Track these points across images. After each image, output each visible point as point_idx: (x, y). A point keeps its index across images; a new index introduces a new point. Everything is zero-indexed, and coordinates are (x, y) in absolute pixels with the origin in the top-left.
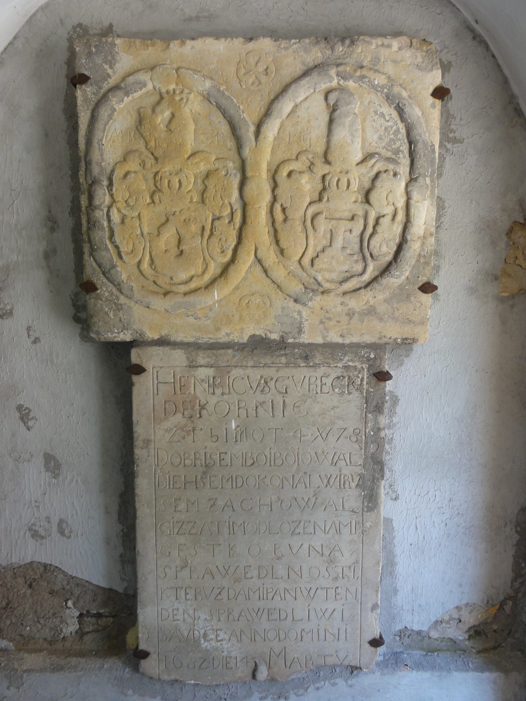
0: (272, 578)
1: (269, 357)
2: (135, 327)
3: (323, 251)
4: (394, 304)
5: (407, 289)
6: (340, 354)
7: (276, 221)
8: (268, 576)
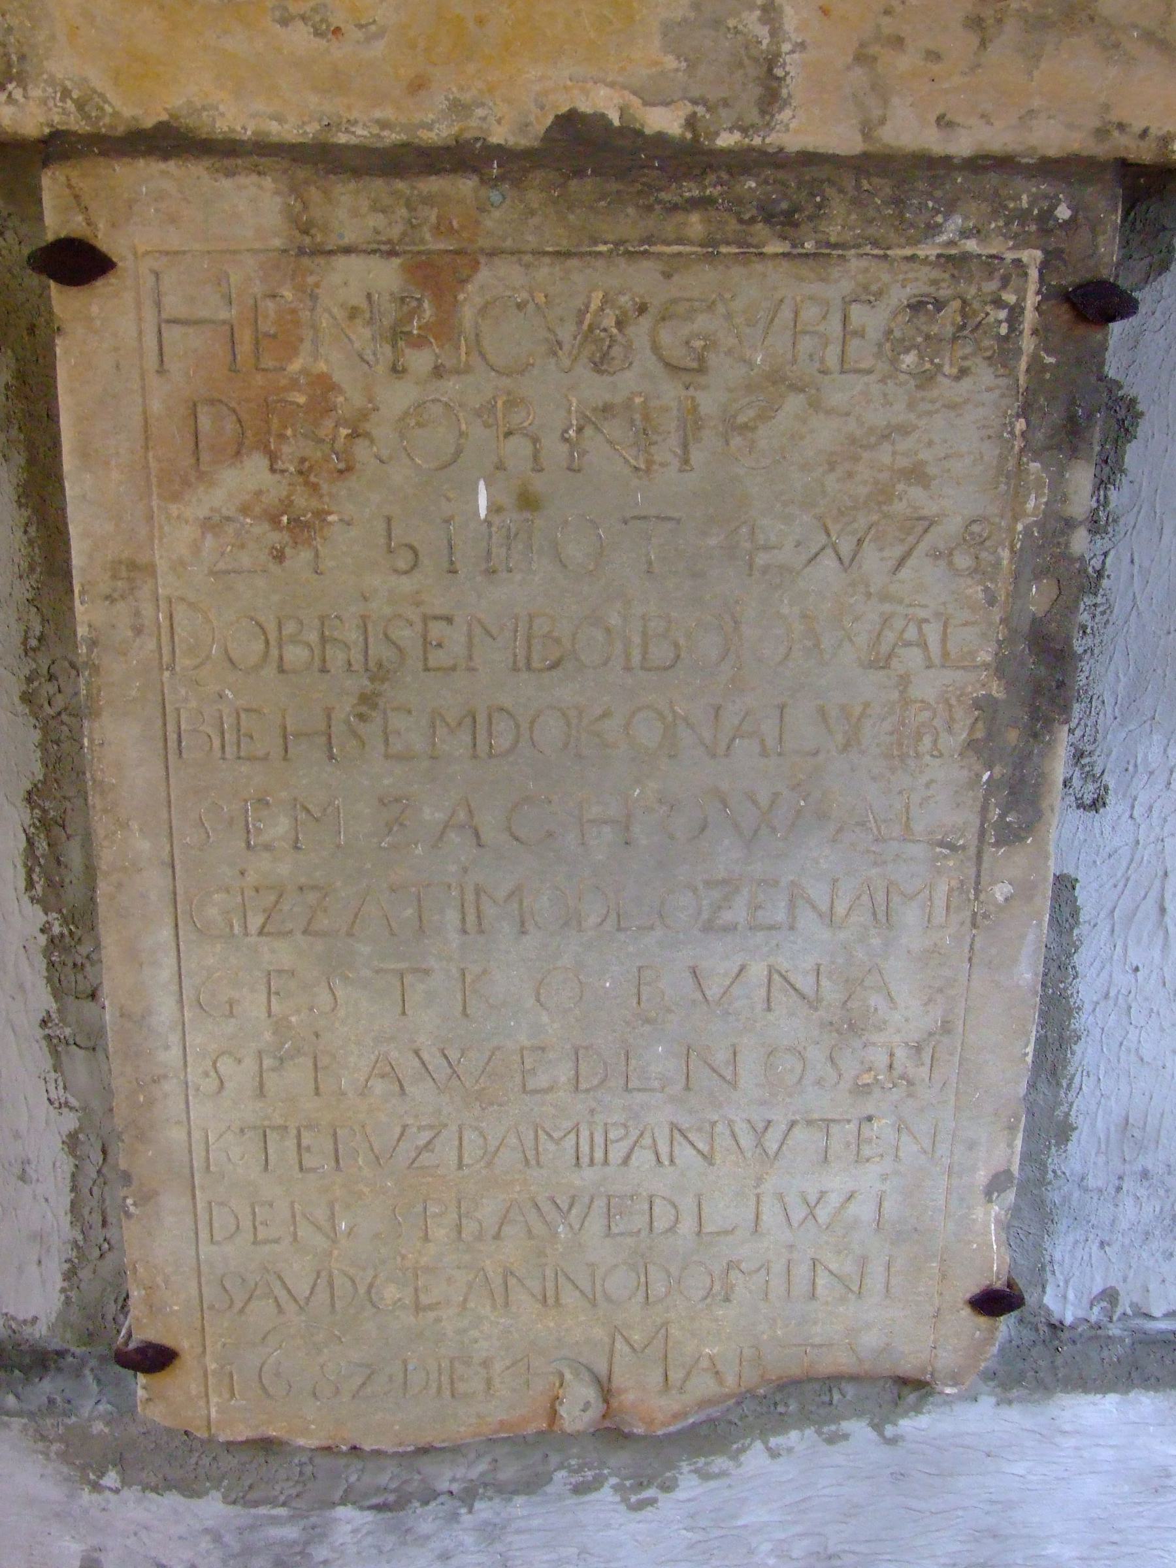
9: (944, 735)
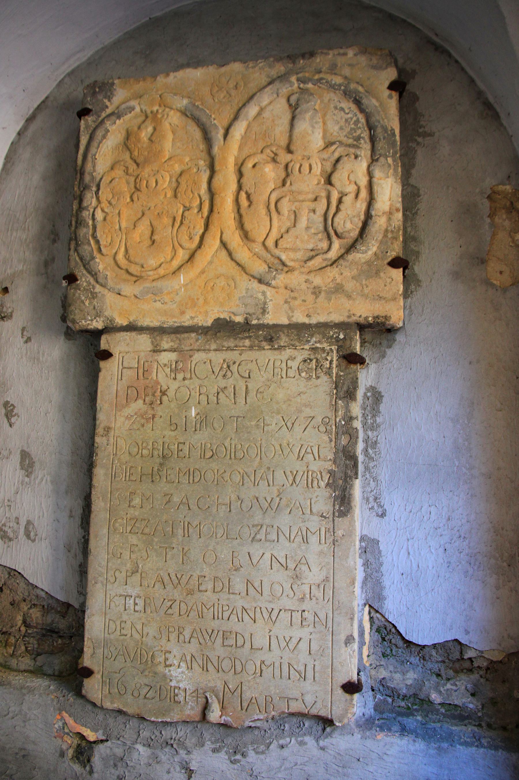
0: (229, 593)
1: (232, 340)
2: (106, 314)
3: (287, 232)
4: (362, 281)
5: (376, 265)
6: (306, 335)
7: (241, 207)
8: (224, 590)
9: (320, 481)
